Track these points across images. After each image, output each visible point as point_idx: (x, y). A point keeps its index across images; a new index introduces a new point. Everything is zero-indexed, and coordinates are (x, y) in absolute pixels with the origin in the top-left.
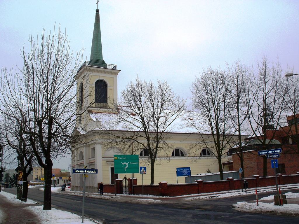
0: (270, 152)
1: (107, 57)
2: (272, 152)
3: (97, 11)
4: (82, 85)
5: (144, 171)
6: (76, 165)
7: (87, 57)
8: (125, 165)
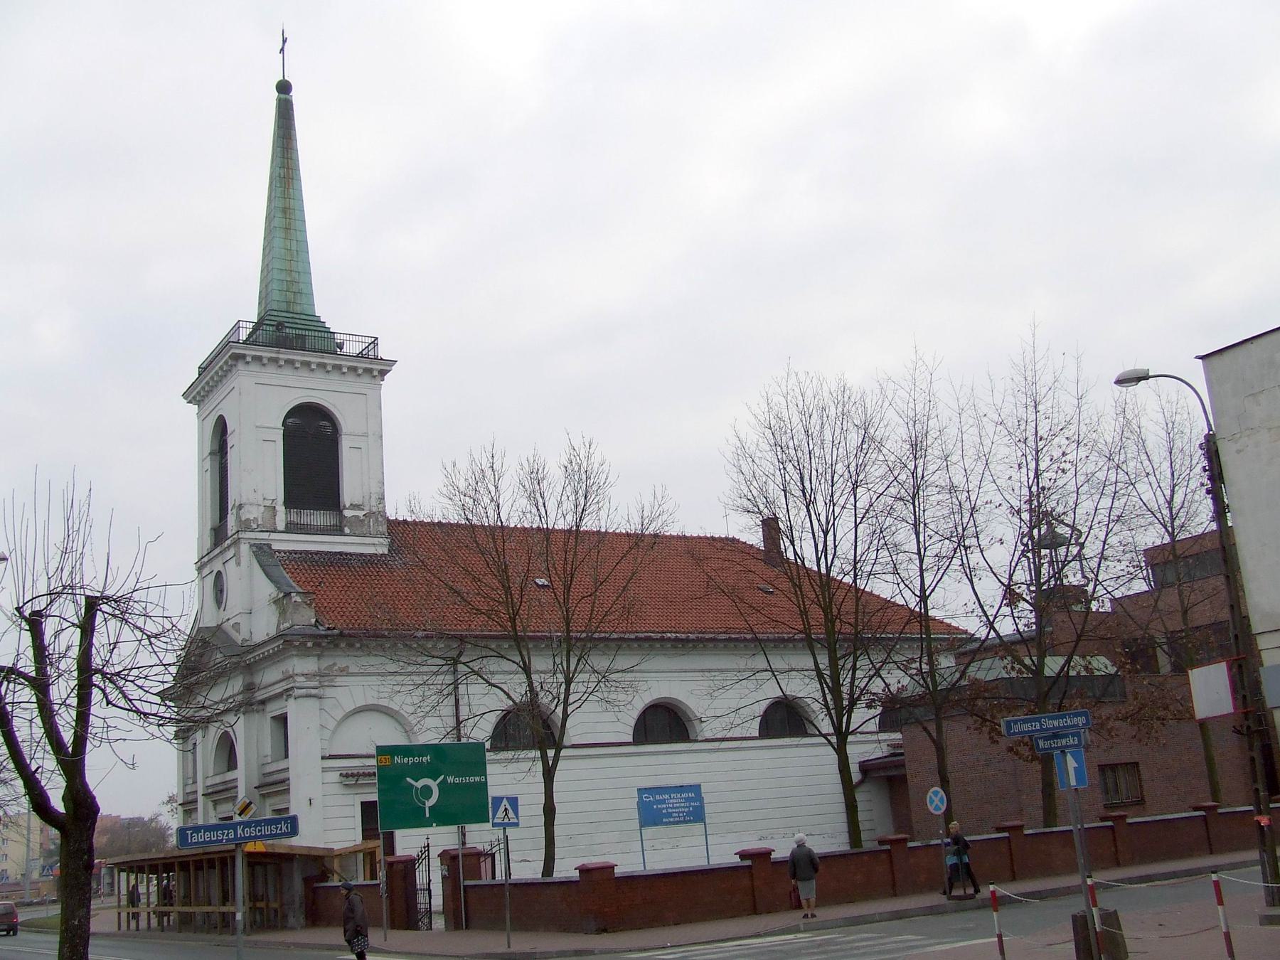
0: (1050, 724)
1: (337, 307)
2: (1056, 723)
3: (284, 87)
4: (221, 428)
5: (511, 814)
6: (200, 799)
7: (246, 309)
8: (427, 791)
